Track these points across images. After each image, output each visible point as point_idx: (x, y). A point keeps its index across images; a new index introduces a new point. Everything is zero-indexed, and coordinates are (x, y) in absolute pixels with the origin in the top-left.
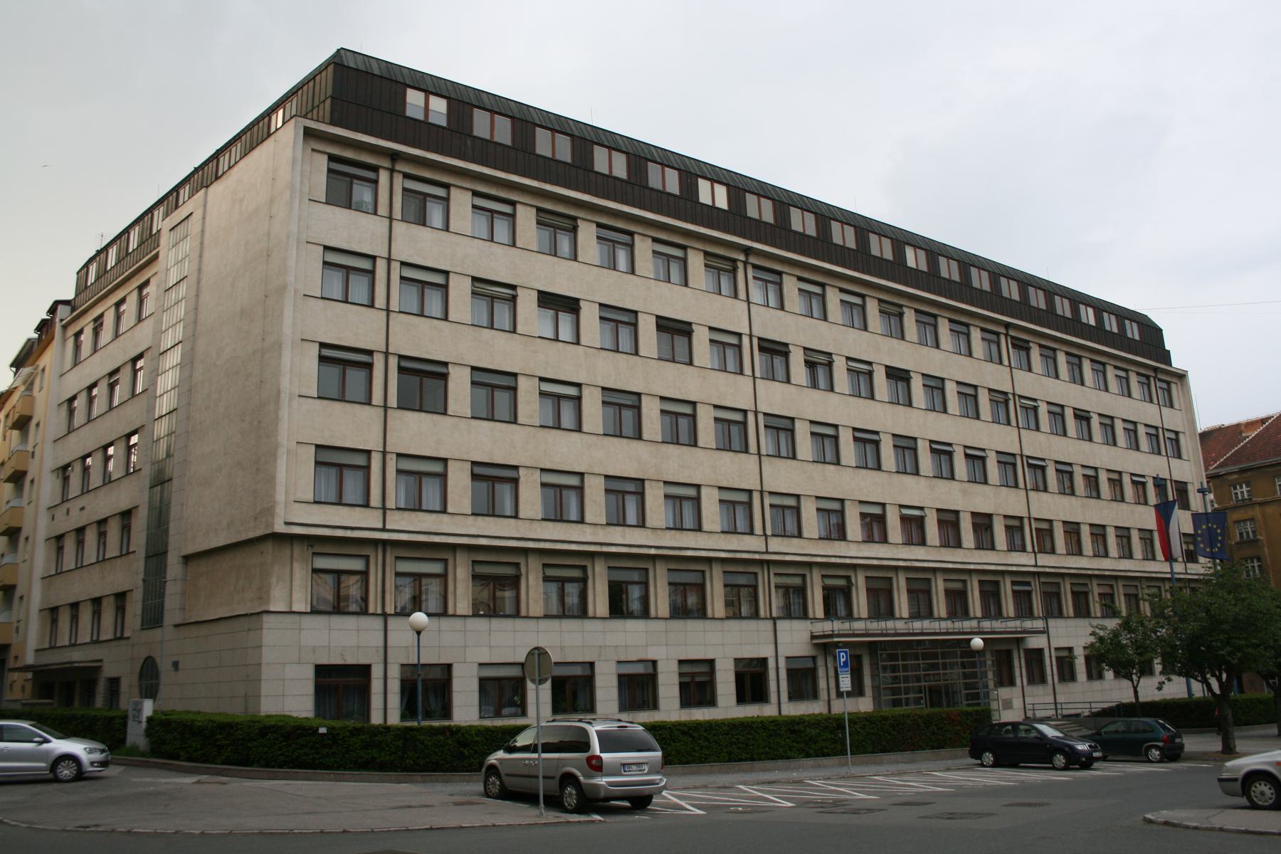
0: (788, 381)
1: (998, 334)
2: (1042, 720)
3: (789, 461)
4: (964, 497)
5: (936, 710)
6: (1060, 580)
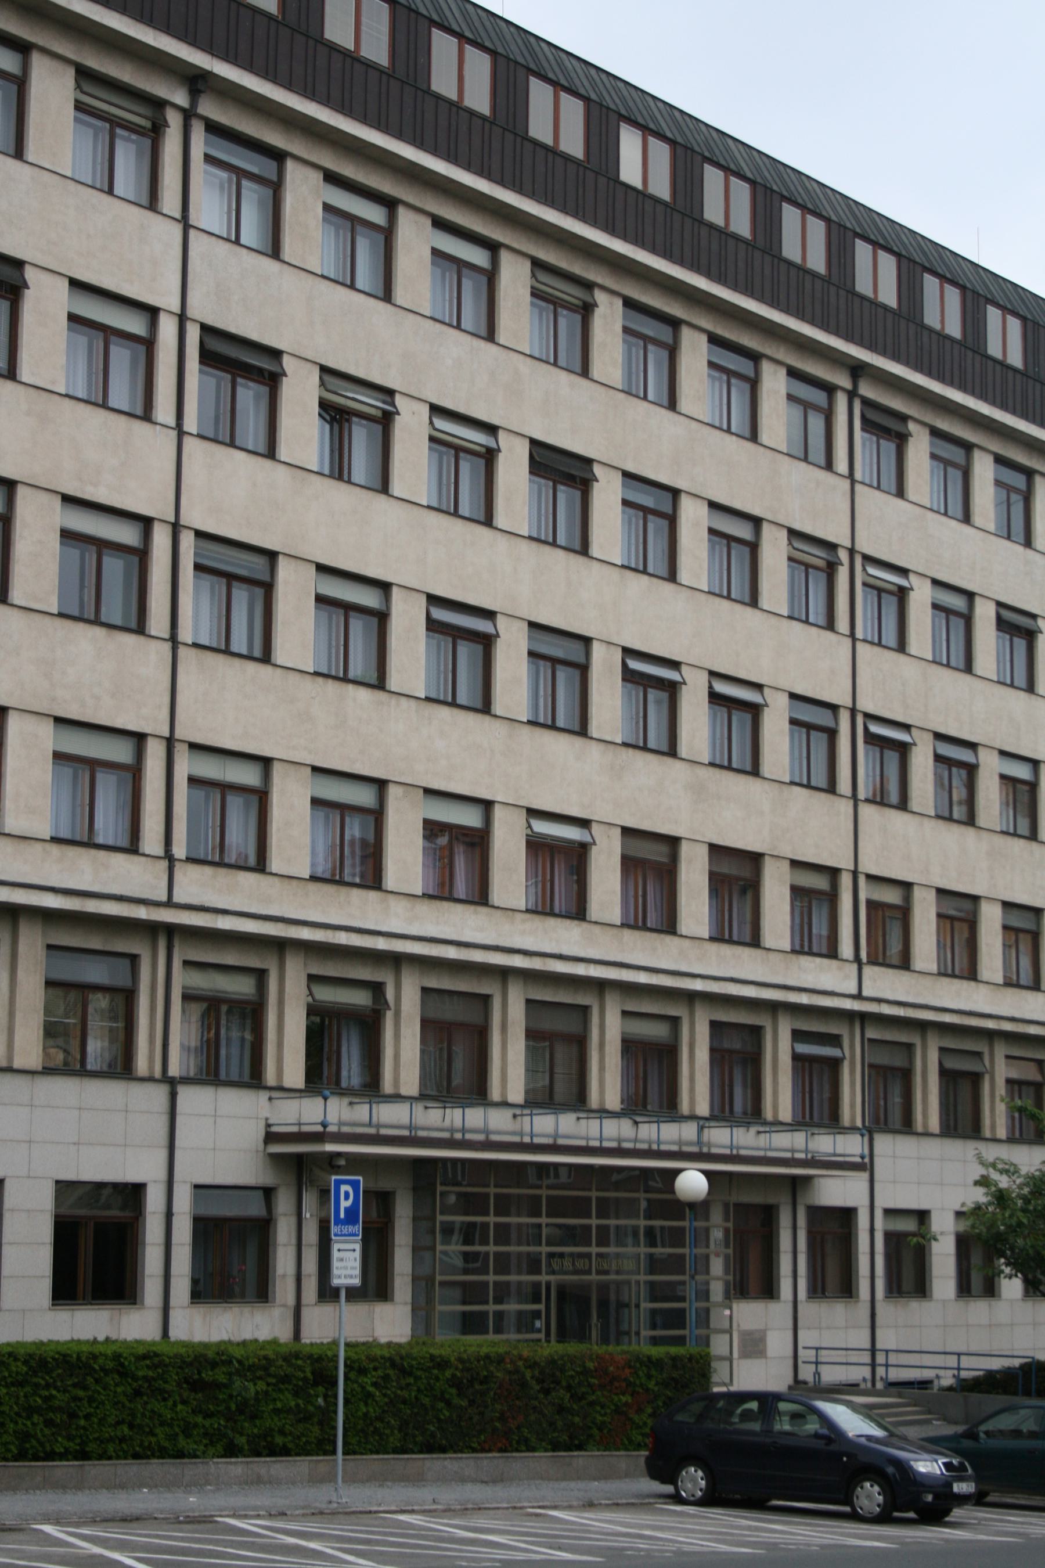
0: (271, 453)
1: (830, 389)
2: (835, 1392)
3: (251, 667)
4: (699, 806)
5: (572, 1348)
6: (915, 1039)
